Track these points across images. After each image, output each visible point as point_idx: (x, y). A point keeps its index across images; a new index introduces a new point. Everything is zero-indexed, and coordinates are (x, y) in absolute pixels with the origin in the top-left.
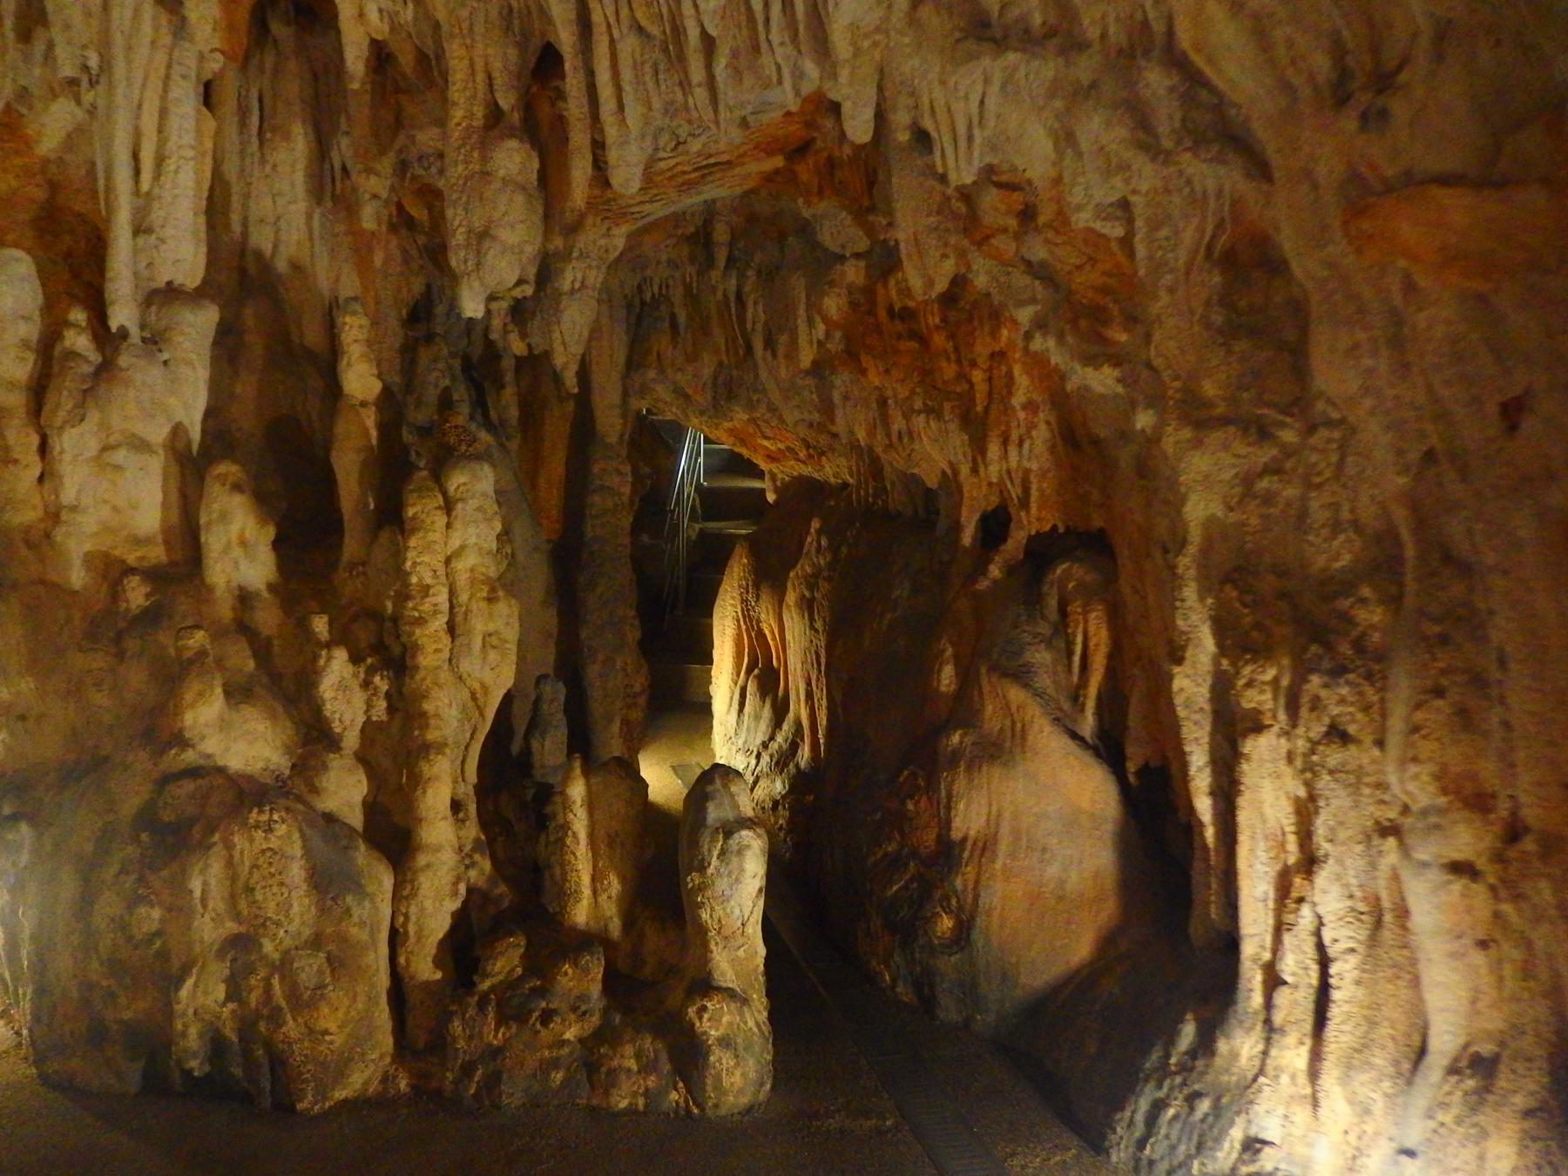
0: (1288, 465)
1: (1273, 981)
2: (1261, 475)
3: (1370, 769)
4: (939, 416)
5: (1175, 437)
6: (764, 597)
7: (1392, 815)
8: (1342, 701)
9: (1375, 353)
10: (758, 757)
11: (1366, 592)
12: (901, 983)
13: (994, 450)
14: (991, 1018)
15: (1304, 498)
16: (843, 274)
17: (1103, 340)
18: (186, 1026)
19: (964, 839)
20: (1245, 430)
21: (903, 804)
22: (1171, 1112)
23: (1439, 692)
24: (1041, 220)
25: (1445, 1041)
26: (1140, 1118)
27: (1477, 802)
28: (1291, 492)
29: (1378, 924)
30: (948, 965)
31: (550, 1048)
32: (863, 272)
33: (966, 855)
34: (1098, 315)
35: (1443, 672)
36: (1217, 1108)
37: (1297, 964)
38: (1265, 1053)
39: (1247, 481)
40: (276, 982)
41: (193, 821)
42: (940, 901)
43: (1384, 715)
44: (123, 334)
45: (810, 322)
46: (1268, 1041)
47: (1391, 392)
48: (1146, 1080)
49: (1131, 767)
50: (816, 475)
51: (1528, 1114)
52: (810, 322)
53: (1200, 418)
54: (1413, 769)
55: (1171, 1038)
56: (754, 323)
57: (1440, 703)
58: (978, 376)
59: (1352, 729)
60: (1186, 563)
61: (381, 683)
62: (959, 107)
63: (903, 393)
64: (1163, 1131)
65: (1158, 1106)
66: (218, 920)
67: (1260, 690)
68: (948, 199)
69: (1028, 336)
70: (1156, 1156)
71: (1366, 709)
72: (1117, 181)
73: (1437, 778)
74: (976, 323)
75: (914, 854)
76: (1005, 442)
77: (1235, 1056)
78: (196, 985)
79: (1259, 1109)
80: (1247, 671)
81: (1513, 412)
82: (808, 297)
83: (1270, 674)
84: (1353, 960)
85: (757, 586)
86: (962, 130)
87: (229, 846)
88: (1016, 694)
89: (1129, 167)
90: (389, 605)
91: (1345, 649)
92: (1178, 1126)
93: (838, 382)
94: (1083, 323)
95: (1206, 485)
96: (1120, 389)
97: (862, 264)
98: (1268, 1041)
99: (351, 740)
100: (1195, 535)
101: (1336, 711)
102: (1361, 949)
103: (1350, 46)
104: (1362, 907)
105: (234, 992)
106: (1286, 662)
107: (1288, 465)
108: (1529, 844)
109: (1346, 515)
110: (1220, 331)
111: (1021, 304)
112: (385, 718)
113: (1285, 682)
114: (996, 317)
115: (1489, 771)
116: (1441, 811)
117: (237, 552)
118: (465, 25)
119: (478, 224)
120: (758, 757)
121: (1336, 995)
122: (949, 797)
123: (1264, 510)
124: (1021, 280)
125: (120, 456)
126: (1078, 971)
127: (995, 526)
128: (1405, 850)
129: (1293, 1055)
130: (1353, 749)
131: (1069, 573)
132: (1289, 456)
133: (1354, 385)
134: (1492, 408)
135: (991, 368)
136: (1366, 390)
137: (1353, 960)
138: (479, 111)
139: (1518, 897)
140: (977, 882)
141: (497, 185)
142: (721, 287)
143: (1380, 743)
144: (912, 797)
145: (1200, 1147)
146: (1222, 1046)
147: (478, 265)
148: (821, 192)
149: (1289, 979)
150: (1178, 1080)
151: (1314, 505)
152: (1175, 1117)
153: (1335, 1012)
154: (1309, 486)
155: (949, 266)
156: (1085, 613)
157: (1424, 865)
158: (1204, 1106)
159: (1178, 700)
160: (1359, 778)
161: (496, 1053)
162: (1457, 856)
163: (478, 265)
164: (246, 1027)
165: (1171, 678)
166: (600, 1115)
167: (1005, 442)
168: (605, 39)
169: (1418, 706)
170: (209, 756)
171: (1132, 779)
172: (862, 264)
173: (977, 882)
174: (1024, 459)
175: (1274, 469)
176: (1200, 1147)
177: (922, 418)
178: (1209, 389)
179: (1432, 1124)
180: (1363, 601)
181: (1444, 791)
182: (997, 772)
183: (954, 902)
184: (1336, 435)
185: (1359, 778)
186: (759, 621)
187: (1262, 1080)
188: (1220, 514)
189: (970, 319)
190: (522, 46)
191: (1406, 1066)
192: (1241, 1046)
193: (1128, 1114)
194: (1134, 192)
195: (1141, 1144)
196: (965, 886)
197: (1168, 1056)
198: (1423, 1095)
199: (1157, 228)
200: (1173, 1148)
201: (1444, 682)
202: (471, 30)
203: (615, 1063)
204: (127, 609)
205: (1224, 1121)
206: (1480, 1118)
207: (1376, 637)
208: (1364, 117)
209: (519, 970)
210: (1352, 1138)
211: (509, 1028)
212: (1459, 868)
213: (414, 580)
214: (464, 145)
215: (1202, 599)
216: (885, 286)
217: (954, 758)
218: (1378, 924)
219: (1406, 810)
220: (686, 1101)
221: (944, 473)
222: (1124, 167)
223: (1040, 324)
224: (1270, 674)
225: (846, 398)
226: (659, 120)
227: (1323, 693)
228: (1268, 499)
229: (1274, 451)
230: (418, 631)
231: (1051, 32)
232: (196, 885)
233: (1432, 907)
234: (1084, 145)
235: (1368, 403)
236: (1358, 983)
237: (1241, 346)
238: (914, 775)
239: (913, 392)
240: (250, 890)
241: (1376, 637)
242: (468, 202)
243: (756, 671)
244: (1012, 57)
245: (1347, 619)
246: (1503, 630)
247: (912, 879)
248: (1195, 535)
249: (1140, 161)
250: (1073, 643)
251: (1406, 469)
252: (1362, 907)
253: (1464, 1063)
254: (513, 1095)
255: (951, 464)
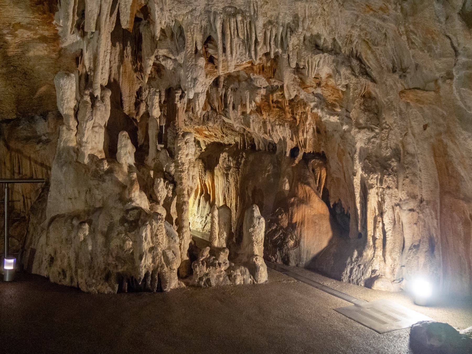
0: (377, 136)
1: (374, 239)
2: (372, 138)
3: (394, 193)
4: (283, 125)
5: (354, 130)
6: (207, 174)
7: (398, 202)
8: (390, 180)
9: (397, 116)
10: (206, 218)
11: (393, 160)
12: (278, 260)
13: (300, 134)
14: (304, 263)
15: (381, 142)
16: (260, 92)
17: (335, 111)
18: (142, 270)
19: (296, 222)
20: (369, 129)
21: (278, 216)
22: (355, 269)
23: (407, 177)
24: (322, 85)
25: (408, 244)
26: (348, 272)
27: (413, 197)
28: (378, 141)
29: (395, 224)
30: (292, 253)
31: (219, 272)
32: (265, 92)
33: (297, 226)
34: (333, 105)
35: (408, 174)
36: (365, 266)
37: (379, 234)
38: (374, 253)
39: (369, 139)
40: (162, 258)
41: (138, 220)
42: (290, 237)
43: (398, 182)
44: (97, 97)
45: (250, 102)
46: (375, 251)
47: (399, 123)
48: (348, 264)
49: (332, 204)
50: (221, 142)
51: (426, 252)
52: (250, 102)
53: (360, 128)
54: (403, 192)
55: (352, 256)
56: (230, 102)
57: (407, 179)
58: (298, 117)
59: (391, 186)
60: (356, 156)
61: (171, 187)
62: (314, 63)
63: (272, 120)
64: (354, 273)
65: (352, 270)
66: (148, 243)
67: (373, 179)
68: (296, 78)
69: (312, 109)
70: (354, 278)
71: (394, 182)
72: (347, 81)
73: (407, 193)
74: (299, 105)
75: (282, 228)
76: (303, 132)
77: (367, 255)
78: (145, 259)
79: (374, 264)
80: (371, 176)
81: (425, 127)
82: (250, 97)
83: (376, 176)
84: (391, 231)
85: (205, 171)
86: (314, 67)
87: (151, 225)
88: (308, 188)
89: (350, 78)
90: (164, 169)
91: (390, 170)
92: (357, 271)
93: (252, 117)
94: (330, 107)
95: (361, 140)
96: (338, 121)
97: (265, 90)
98: (375, 251)
99: (162, 203)
100: (358, 150)
101: (389, 182)
102: (392, 230)
103: (396, 63)
104: (391, 221)
105: (153, 261)
106: (379, 173)
107: (377, 136)
108: (424, 203)
109: (389, 145)
110: (363, 110)
111: (311, 102)
112: (171, 196)
113: (379, 177)
114: (305, 105)
115: (417, 191)
116: (408, 200)
117: (128, 155)
118: (192, 30)
119: (194, 77)
120: (206, 218)
121: (388, 239)
122: (292, 213)
123: (373, 145)
124: (311, 97)
125: (96, 129)
126: (324, 249)
127: (295, 151)
128: (401, 208)
129: (379, 252)
130: (391, 190)
131: (314, 162)
132: (377, 135)
133: (392, 122)
134: (422, 126)
135: (301, 115)
136: (395, 122)
137: (391, 231)
138: (194, 50)
139: (423, 213)
140: (301, 231)
141: (199, 67)
142: (221, 92)
143: (397, 188)
144: (280, 215)
145: (363, 274)
146: (365, 254)
147: (194, 86)
148: (259, 73)
149: (378, 238)
150: (355, 263)
151: (383, 144)
152: (356, 270)
153: (388, 242)
154: (382, 140)
155: (295, 93)
156: (321, 170)
157: (405, 210)
158: (362, 267)
159: (355, 184)
160: (392, 196)
161: (207, 275)
162: (410, 208)
163: (194, 86)
164: (154, 271)
165: (353, 179)
166: (235, 286)
167: (303, 132)
168: (230, 37)
169: (404, 180)
170: (138, 204)
171: (332, 206)
172: (265, 90)
173: (301, 231)
174: (308, 135)
175: (374, 137)
176: (363, 274)
177: (278, 126)
178: (361, 121)
179: (407, 260)
180: (393, 161)
181: (408, 196)
182: (304, 206)
183: (294, 237)
184: (388, 130)
185: (392, 196)
186: (205, 181)
187: (374, 258)
188: (363, 146)
189: (297, 104)
190: (204, 35)
191: (401, 251)
192: (369, 253)
193: (345, 272)
194: (351, 83)
195: (350, 277)
196: (297, 233)
197: (352, 259)
198: (405, 256)
199: (355, 90)
200: (357, 276)
201: (408, 175)
202: (193, 30)
203: (235, 274)
204: (103, 169)
205: (367, 268)
206: (417, 255)
207: (395, 168)
208: (400, 77)
209: (209, 255)
210: (392, 266)
211: (210, 268)
212: (411, 210)
213: (180, 161)
214: (191, 57)
215: (359, 163)
216: (272, 95)
217: (292, 205)
218: (395, 224)
219: (401, 200)
220: (253, 281)
221: (280, 139)
222: (349, 78)
223: (316, 106)
224: (376, 176)
225: (253, 121)
226: (238, 56)
227: (387, 179)
228: (373, 143)
229: (375, 134)
230: (182, 174)
231: (332, 50)
232: (144, 235)
233: (405, 217)
234: (342, 73)
235: (395, 125)
236: (392, 236)
237: (366, 113)
238: (280, 210)
239: (275, 120)
240: (156, 235)
241: (395, 168)
242: (192, 71)
243: (203, 195)
244: (326, 54)
245: (390, 165)
246: (420, 165)
247: (281, 234)
248: (358, 150)
249: (353, 77)
250: (317, 177)
251: (402, 137)
252: (391, 221)
253: (412, 247)
254: (213, 283)
255: (283, 137)
